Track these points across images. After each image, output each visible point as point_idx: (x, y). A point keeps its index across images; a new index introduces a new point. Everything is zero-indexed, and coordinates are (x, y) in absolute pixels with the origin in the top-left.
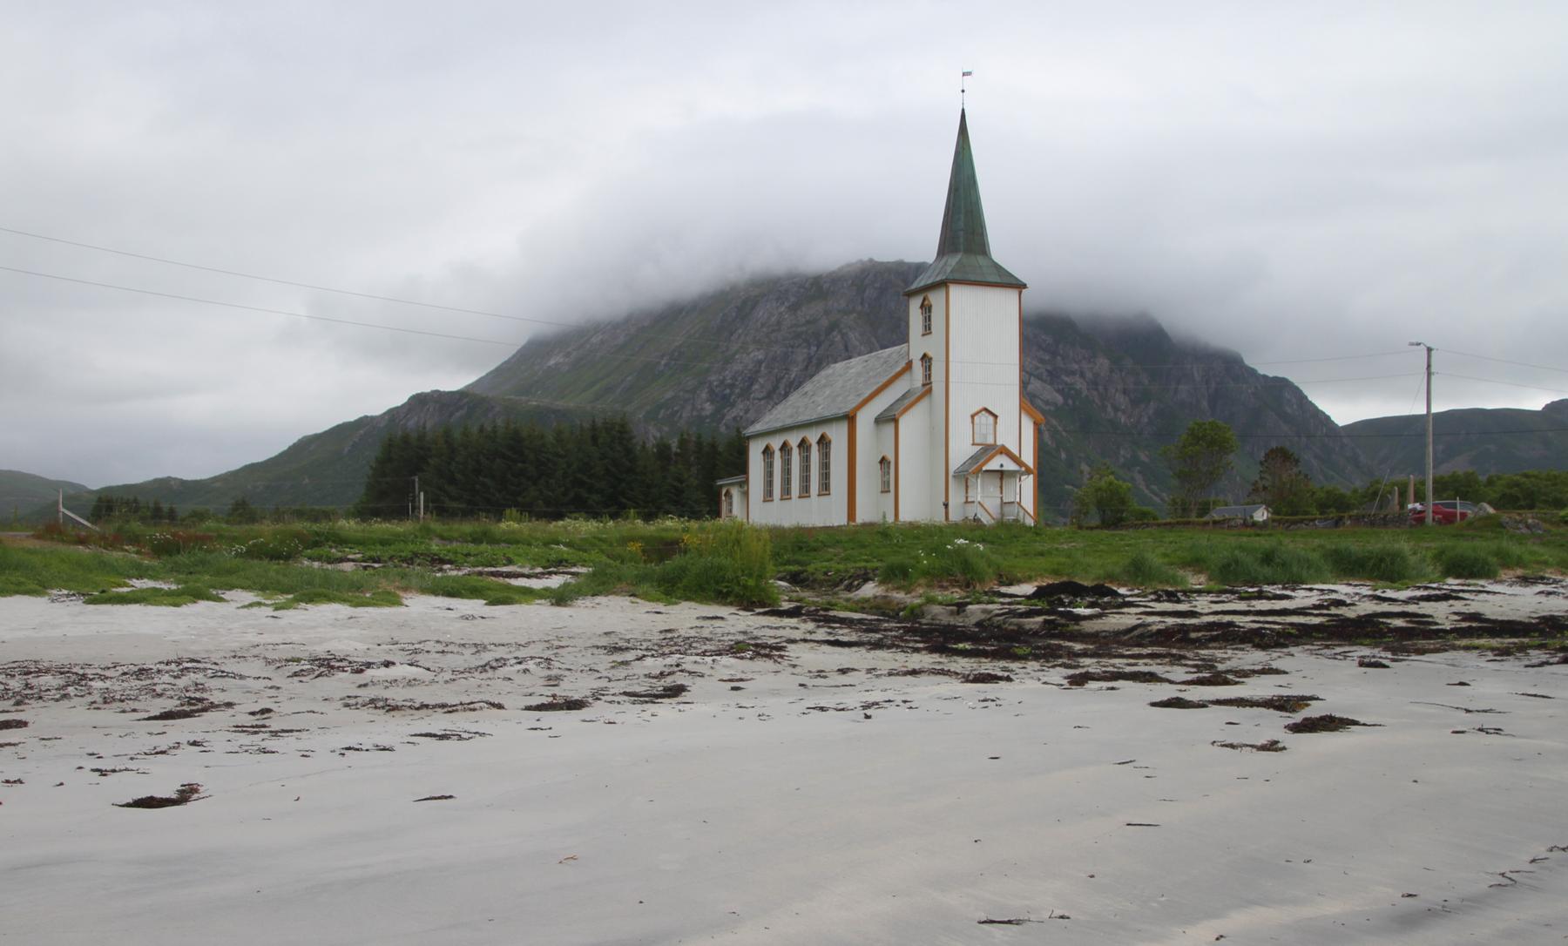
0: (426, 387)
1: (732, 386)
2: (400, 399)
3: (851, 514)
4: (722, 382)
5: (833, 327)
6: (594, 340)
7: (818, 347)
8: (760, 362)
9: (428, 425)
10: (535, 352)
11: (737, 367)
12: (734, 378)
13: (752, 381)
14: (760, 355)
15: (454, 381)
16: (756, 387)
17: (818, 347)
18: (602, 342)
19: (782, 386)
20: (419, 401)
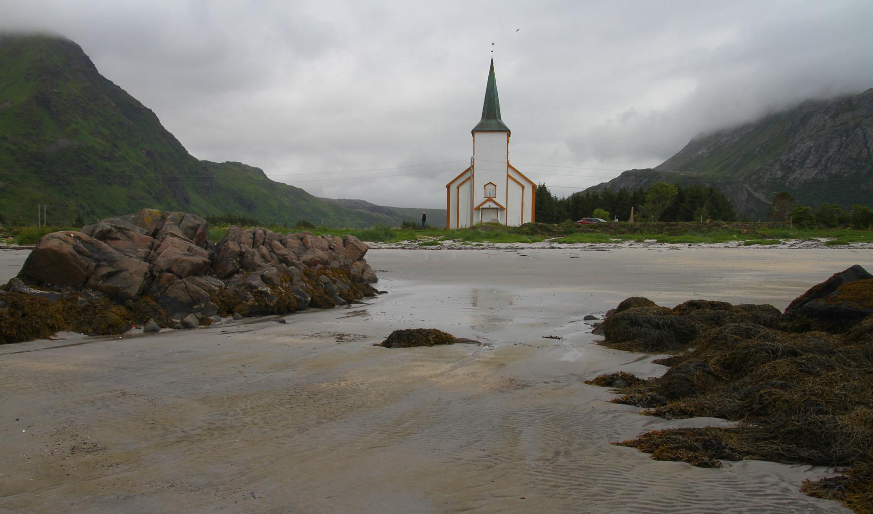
0: (630, 168)
1: (794, 161)
2: (617, 175)
3: (472, 221)
4: (788, 160)
5: (857, 125)
6: (722, 140)
7: (847, 137)
8: (811, 148)
9: (630, 187)
10: (693, 146)
11: (798, 151)
12: (795, 157)
13: (806, 158)
14: (811, 144)
15: (652, 164)
16: (808, 161)
17: (847, 137)
18: (727, 141)
19: (823, 160)
20: (626, 175)
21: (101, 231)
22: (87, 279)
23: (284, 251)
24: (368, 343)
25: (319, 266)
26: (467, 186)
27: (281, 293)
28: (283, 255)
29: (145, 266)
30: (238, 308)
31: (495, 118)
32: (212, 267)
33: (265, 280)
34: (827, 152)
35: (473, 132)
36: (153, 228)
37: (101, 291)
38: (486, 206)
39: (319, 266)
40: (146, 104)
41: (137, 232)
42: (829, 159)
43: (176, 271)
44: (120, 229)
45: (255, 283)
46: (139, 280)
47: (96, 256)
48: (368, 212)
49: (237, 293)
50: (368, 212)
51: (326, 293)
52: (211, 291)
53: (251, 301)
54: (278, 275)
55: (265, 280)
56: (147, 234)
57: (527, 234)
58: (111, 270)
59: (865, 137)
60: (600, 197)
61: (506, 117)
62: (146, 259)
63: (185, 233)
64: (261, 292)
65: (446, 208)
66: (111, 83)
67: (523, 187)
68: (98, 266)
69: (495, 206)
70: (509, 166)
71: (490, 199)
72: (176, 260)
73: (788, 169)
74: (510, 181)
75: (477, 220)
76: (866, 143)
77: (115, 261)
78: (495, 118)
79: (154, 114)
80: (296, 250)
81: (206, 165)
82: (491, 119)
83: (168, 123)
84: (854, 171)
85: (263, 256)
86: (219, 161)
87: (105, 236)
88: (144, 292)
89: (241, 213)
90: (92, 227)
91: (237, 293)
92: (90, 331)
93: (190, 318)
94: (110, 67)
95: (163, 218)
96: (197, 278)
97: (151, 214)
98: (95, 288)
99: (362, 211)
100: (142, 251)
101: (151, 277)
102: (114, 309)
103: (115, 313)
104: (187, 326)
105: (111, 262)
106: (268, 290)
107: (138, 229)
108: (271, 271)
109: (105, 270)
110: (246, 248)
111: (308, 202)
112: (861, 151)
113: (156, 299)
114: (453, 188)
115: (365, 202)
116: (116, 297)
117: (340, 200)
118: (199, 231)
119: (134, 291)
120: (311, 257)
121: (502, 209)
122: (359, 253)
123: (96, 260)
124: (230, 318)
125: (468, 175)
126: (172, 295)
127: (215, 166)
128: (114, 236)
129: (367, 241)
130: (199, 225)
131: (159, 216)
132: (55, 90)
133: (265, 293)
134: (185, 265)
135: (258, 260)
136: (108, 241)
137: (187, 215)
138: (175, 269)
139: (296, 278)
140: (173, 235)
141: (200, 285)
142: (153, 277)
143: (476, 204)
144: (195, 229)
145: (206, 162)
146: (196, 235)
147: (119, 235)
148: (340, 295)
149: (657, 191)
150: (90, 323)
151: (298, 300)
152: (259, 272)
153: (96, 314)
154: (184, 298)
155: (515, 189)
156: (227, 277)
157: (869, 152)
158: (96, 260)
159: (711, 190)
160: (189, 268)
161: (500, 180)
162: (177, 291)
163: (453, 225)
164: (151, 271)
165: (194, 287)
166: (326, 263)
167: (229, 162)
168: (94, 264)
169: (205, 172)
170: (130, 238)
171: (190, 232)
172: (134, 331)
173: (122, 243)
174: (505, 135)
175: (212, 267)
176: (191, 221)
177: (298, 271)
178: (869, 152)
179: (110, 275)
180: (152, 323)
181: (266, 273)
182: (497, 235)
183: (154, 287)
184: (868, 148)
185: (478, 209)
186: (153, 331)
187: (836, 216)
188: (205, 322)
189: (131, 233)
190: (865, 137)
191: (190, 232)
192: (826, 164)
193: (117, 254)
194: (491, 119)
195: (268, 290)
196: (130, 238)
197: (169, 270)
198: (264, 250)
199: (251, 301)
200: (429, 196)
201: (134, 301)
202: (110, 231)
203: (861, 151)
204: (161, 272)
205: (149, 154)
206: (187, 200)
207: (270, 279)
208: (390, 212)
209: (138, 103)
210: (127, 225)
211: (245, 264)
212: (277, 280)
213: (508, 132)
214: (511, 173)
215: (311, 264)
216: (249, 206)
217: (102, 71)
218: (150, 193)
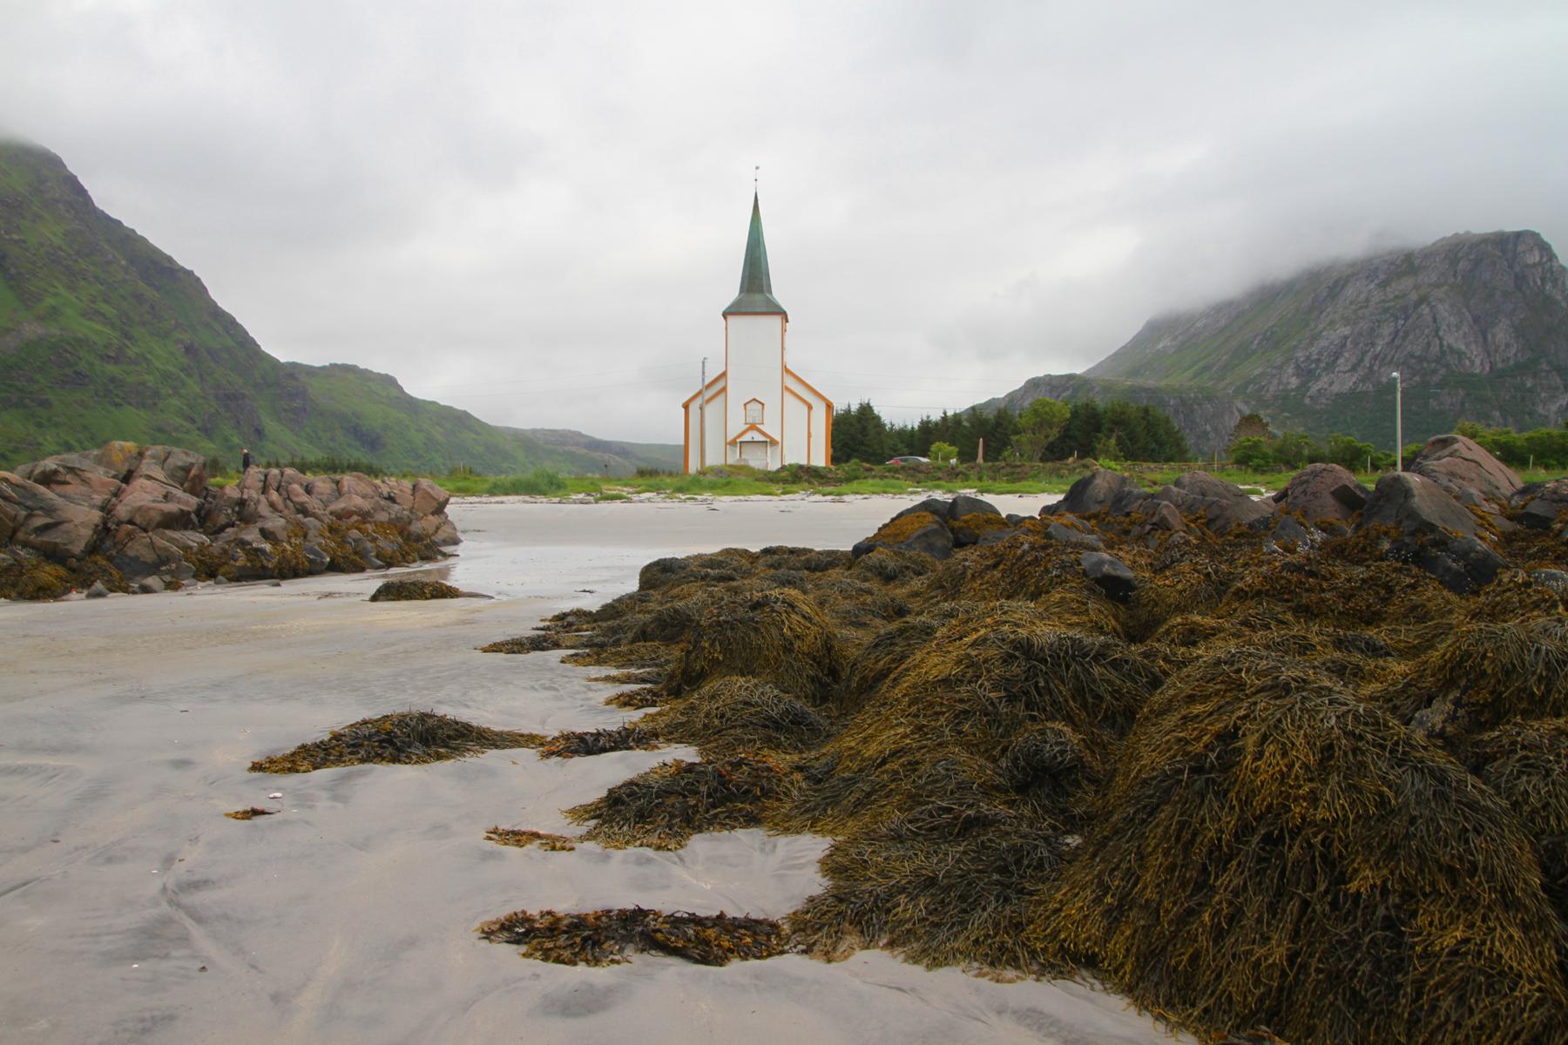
0: (1040, 371)
1: (1318, 360)
4: (1308, 358)
5: (1423, 300)
7: (1406, 319)
8: (1346, 338)
10: (1155, 329)
11: (1323, 343)
12: (1320, 353)
13: (1337, 355)
14: (1346, 331)
15: (1078, 367)
16: (1341, 361)
17: (1406, 319)
18: (1205, 326)
19: (1367, 360)
20: (1034, 384)
21: (43, 473)
22: (15, 531)
23: (304, 498)
24: (358, 599)
25: (355, 518)
26: (719, 400)
27: (285, 550)
28: (302, 504)
29: (96, 516)
30: (222, 570)
31: (762, 291)
32: (202, 519)
33: (266, 534)
34: (1373, 344)
35: (725, 315)
36: (124, 469)
37: (33, 548)
38: (747, 437)
39: (355, 518)
40: (184, 260)
41: (99, 475)
42: (1376, 357)
43: (141, 523)
44: (71, 470)
45: (248, 538)
46: (87, 533)
47: (29, 503)
48: (584, 451)
49: (225, 551)
50: (584, 451)
51: (356, 553)
52: (186, 548)
53: (242, 560)
54: (285, 529)
55: (266, 534)
56: (114, 477)
57: (785, 481)
58: (49, 520)
59: (1435, 320)
60: (966, 424)
61: (780, 291)
62: (102, 509)
63: (172, 476)
64: (257, 550)
65: (682, 442)
66: (119, 223)
67: (810, 407)
68: (29, 516)
69: (762, 439)
70: (786, 370)
71: (753, 427)
72: (140, 508)
73: (1307, 374)
74: (787, 396)
75: (733, 458)
76: (1437, 330)
77: (55, 510)
78: (762, 291)
79: (198, 279)
80: (324, 498)
81: (294, 370)
82: (755, 291)
83: (225, 297)
84: (1417, 379)
85: (272, 505)
86: (317, 362)
87: (48, 479)
88: (93, 549)
89: (361, 455)
90: (30, 466)
91: (225, 551)
92: (13, 595)
93: (152, 581)
94: (115, 196)
95: (141, 455)
96: (169, 533)
97: (122, 449)
98: (25, 545)
99: (573, 449)
100: (98, 499)
101: (104, 531)
102: (47, 568)
103: (48, 573)
104: (146, 590)
105: (49, 510)
106: (267, 547)
107: (101, 470)
108: (275, 523)
109: (39, 521)
110: (253, 494)
111: (478, 433)
112: (1429, 344)
113: (110, 559)
114: (694, 407)
115: (580, 434)
116: (54, 555)
117: (534, 431)
118: (194, 472)
119: (78, 548)
120: (342, 505)
121: (773, 442)
122: (435, 504)
123: (28, 508)
124: (211, 582)
125: (716, 387)
126: (131, 553)
127: (311, 371)
128: (61, 478)
129: (892, 532)
130: (192, 464)
131: (135, 451)
132: (15, 237)
133: (262, 551)
134: (153, 513)
135: (264, 509)
136: (54, 486)
137: (176, 449)
138: (138, 520)
139: (311, 533)
140: (149, 478)
141: (172, 540)
142: (107, 530)
143: (730, 438)
144: (186, 469)
145: (294, 365)
146: (190, 480)
147: (69, 478)
148: (377, 557)
149: (1036, 412)
150: (14, 586)
151: (311, 561)
152: (259, 525)
153: (22, 574)
154: (149, 556)
155: (795, 409)
156: (217, 531)
157: (1441, 345)
158: (28, 508)
159: (1146, 411)
160: (158, 518)
161: (772, 398)
162: (139, 548)
163: (694, 466)
164: (105, 523)
165: (160, 542)
166: (365, 516)
167: (336, 365)
168: (24, 513)
169: (291, 386)
170: (85, 482)
171: (180, 474)
172: (74, 595)
173: (75, 488)
174: (777, 320)
175: (202, 519)
176: (180, 458)
177: (318, 523)
178: (1441, 345)
179: (46, 528)
180: (99, 586)
181: (269, 525)
182: (728, 484)
183: (108, 543)
184: (1441, 339)
185: (733, 443)
186: (99, 595)
187: (1306, 452)
188: (173, 586)
189: (88, 475)
190: (1435, 320)
191: (180, 474)
192: (1372, 366)
193: (59, 501)
194: (755, 291)
195: (267, 547)
196: (85, 482)
197: (131, 522)
198: (274, 496)
199: (242, 560)
200: (646, 417)
201: (79, 560)
202: (56, 472)
203: (1429, 344)
204: (119, 523)
205: (189, 350)
206: (259, 432)
207: (272, 533)
208: (623, 450)
209: (170, 259)
210: (86, 464)
211: (244, 512)
212: (282, 535)
213: (783, 314)
214: (790, 383)
215: (341, 515)
216: (372, 442)
217: (100, 203)
218: (193, 421)
